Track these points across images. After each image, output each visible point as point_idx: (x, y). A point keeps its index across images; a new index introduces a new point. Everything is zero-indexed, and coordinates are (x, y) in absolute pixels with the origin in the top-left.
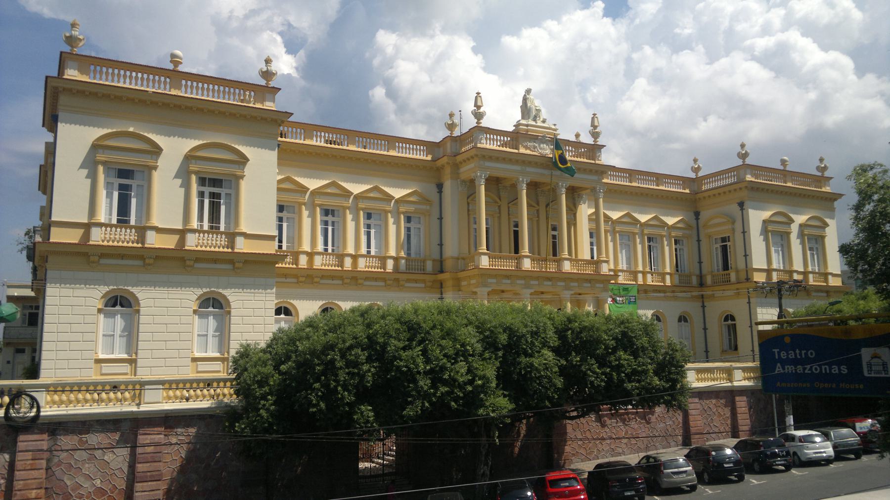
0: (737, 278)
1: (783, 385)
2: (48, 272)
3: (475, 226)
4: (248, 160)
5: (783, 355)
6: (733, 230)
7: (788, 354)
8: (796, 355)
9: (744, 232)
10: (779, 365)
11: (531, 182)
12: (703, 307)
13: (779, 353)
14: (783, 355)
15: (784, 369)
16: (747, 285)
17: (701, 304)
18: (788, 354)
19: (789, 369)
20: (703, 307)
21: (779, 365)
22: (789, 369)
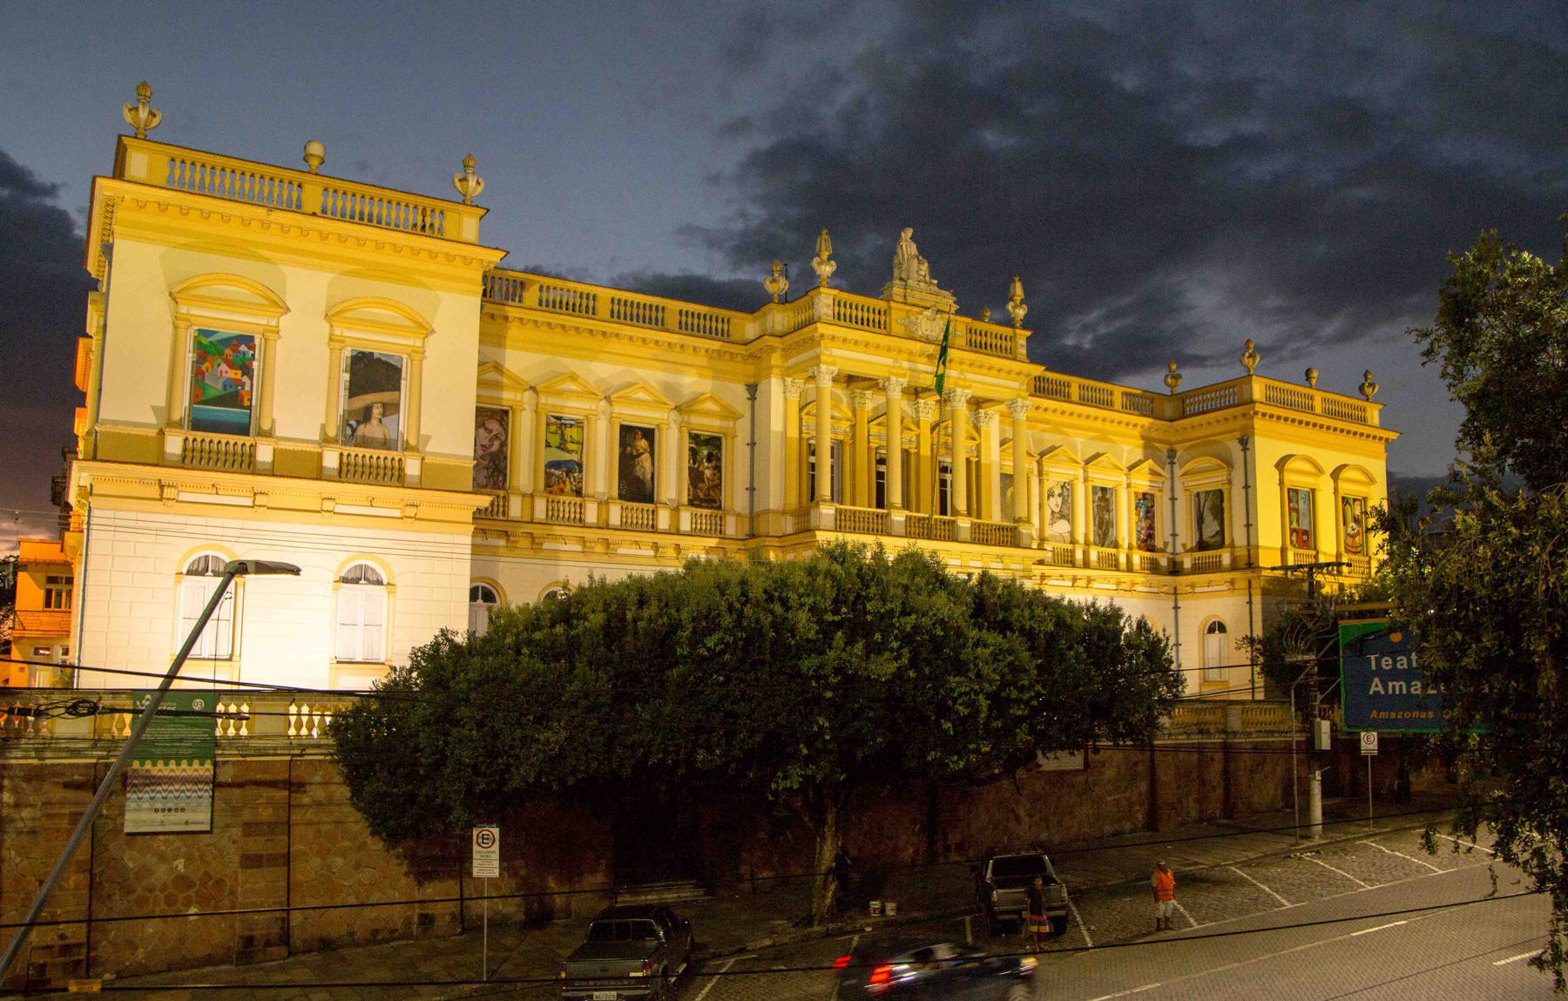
0: (1234, 559)
1: (1383, 715)
2: (95, 513)
3: (812, 459)
4: (398, 371)
5: (1386, 663)
6: (1230, 482)
7: (1395, 662)
8: (1409, 661)
9: (1246, 487)
10: (1376, 680)
11: (909, 387)
12: (1176, 608)
13: (1378, 661)
14: (1386, 663)
15: (1385, 687)
16: (1249, 574)
17: (1172, 604)
18: (1395, 662)
19: (1397, 686)
20: (1176, 608)
21: (1376, 680)
22: (1397, 686)
